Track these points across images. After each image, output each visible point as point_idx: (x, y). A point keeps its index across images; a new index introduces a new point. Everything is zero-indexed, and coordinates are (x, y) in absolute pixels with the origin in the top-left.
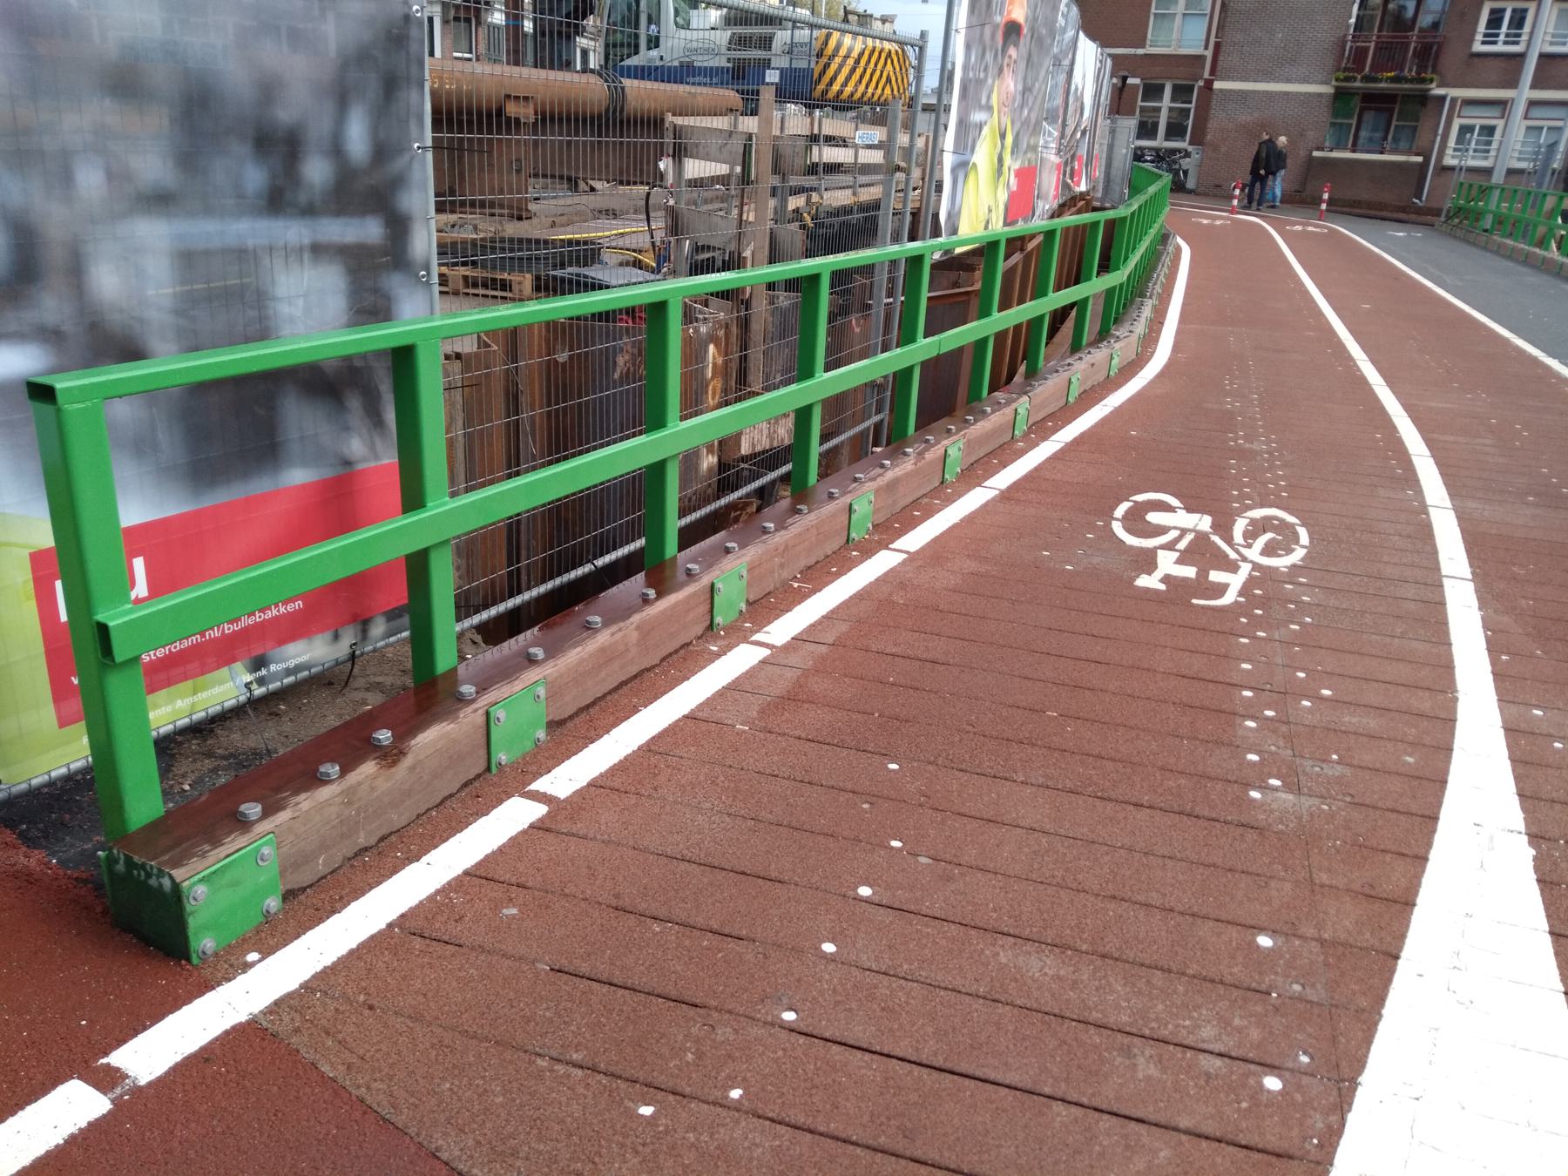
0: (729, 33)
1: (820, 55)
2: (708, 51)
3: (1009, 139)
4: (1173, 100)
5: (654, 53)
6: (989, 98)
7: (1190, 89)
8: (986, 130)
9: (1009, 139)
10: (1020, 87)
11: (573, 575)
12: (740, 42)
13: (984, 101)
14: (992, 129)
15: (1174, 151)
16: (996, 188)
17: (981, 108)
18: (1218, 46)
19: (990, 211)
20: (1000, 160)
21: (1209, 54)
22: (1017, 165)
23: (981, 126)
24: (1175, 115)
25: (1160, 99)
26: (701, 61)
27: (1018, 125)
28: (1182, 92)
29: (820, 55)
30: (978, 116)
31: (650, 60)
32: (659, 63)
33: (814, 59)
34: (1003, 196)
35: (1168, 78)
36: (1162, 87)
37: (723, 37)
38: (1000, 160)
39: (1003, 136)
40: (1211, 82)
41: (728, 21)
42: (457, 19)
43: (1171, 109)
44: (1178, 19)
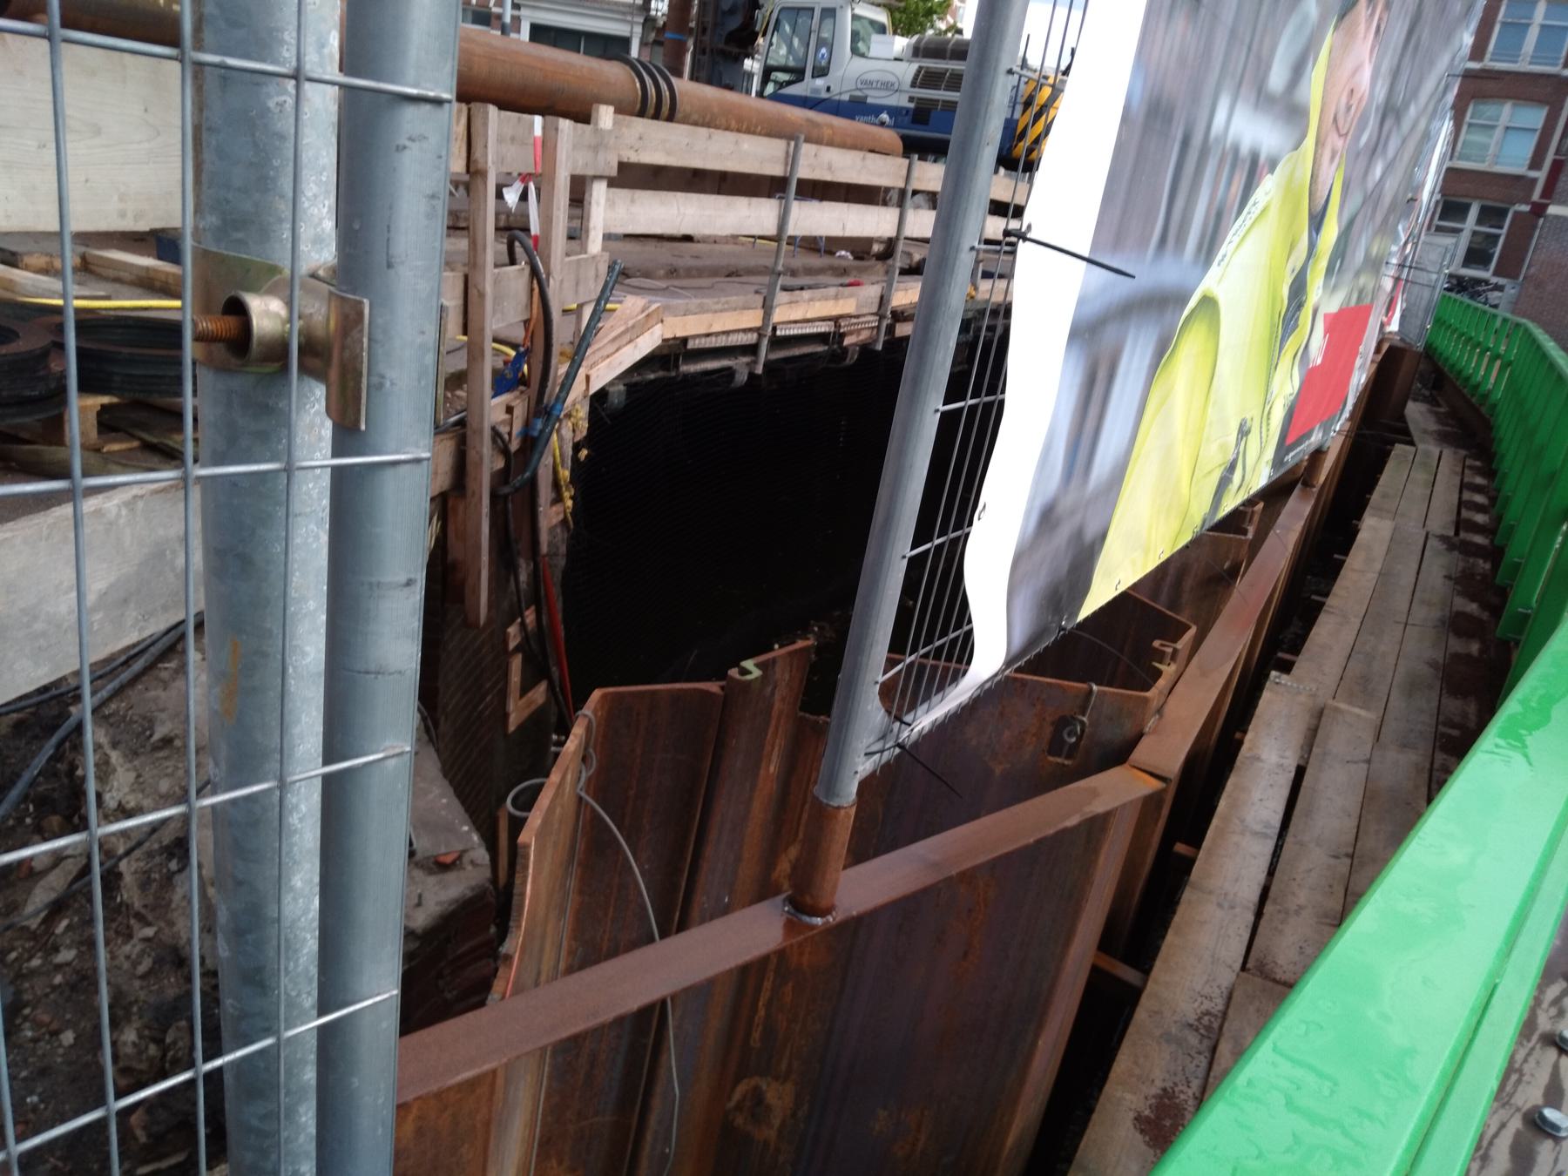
0: (914, 67)
1: (1028, 103)
2: (886, 86)
3: (1331, 232)
4: (1479, 221)
5: (820, 82)
6: (1298, 70)
7: (1502, 213)
8: (1268, 189)
9: (1331, 232)
10: (1381, 94)
11: (678, 686)
12: (926, 79)
13: (1277, 79)
14: (1289, 189)
15: (1478, 282)
16: (1272, 367)
17: (1263, 100)
18: (1557, 167)
19: (1243, 432)
20: (1298, 289)
21: (1541, 175)
22: (1333, 305)
23: (1253, 169)
24: (1479, 239)
25: (1463, 218)
26: (874, 98)
27: (1356, 199)
28: (1491, 215)
29: (1028, 103)
30: (1243, 126)
31: (817, 90)
32: (824, 95)
33: (1019, 108)
34: (1287, 384)
35: (1476, 198)
36: (1467, 207)
37: (908, 70)
38: (1298, 289)
39: (1317, 222)
40: (1545, 206)
41: (917, 52)
42: (657, 43)
43: (1475, 233)
44: (1498, 132)
